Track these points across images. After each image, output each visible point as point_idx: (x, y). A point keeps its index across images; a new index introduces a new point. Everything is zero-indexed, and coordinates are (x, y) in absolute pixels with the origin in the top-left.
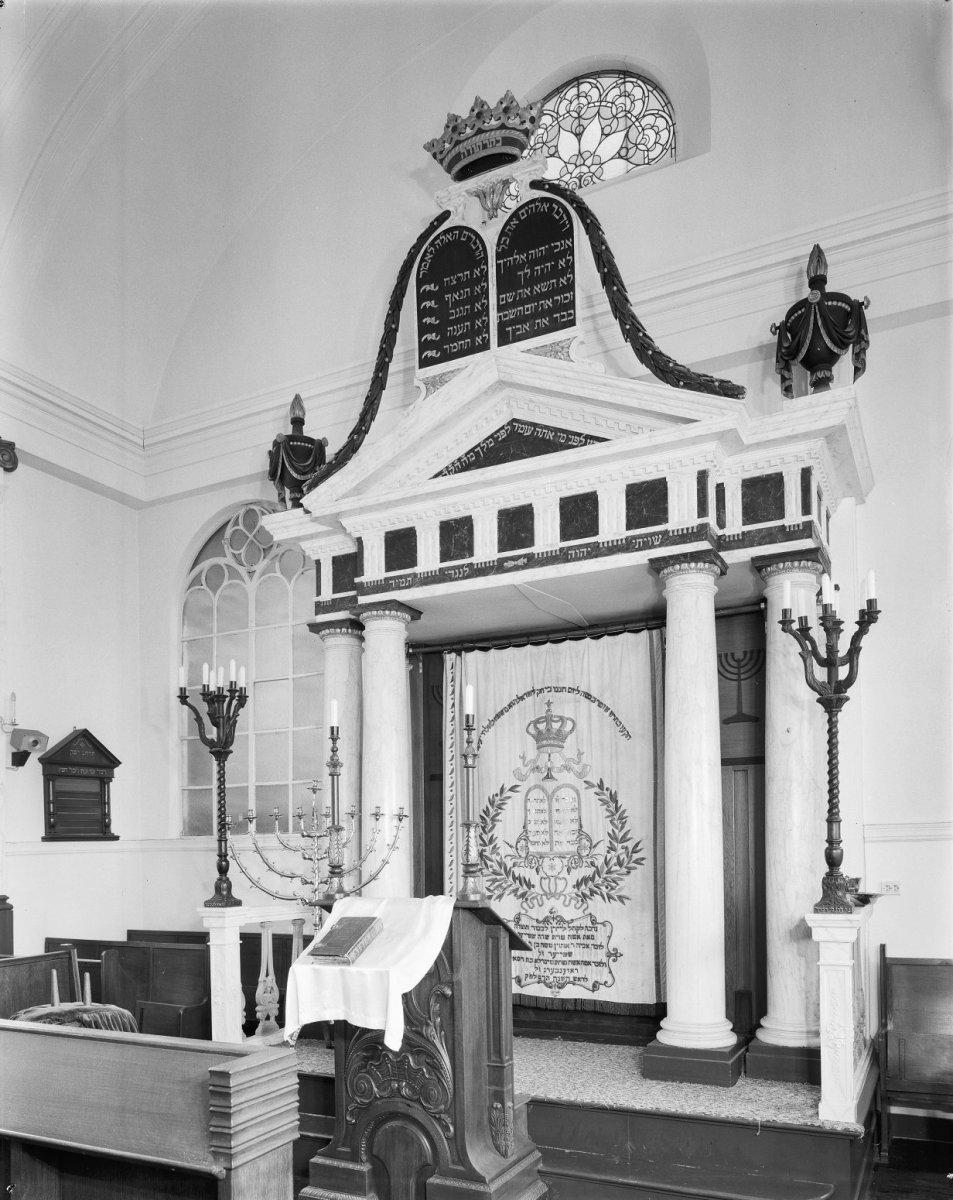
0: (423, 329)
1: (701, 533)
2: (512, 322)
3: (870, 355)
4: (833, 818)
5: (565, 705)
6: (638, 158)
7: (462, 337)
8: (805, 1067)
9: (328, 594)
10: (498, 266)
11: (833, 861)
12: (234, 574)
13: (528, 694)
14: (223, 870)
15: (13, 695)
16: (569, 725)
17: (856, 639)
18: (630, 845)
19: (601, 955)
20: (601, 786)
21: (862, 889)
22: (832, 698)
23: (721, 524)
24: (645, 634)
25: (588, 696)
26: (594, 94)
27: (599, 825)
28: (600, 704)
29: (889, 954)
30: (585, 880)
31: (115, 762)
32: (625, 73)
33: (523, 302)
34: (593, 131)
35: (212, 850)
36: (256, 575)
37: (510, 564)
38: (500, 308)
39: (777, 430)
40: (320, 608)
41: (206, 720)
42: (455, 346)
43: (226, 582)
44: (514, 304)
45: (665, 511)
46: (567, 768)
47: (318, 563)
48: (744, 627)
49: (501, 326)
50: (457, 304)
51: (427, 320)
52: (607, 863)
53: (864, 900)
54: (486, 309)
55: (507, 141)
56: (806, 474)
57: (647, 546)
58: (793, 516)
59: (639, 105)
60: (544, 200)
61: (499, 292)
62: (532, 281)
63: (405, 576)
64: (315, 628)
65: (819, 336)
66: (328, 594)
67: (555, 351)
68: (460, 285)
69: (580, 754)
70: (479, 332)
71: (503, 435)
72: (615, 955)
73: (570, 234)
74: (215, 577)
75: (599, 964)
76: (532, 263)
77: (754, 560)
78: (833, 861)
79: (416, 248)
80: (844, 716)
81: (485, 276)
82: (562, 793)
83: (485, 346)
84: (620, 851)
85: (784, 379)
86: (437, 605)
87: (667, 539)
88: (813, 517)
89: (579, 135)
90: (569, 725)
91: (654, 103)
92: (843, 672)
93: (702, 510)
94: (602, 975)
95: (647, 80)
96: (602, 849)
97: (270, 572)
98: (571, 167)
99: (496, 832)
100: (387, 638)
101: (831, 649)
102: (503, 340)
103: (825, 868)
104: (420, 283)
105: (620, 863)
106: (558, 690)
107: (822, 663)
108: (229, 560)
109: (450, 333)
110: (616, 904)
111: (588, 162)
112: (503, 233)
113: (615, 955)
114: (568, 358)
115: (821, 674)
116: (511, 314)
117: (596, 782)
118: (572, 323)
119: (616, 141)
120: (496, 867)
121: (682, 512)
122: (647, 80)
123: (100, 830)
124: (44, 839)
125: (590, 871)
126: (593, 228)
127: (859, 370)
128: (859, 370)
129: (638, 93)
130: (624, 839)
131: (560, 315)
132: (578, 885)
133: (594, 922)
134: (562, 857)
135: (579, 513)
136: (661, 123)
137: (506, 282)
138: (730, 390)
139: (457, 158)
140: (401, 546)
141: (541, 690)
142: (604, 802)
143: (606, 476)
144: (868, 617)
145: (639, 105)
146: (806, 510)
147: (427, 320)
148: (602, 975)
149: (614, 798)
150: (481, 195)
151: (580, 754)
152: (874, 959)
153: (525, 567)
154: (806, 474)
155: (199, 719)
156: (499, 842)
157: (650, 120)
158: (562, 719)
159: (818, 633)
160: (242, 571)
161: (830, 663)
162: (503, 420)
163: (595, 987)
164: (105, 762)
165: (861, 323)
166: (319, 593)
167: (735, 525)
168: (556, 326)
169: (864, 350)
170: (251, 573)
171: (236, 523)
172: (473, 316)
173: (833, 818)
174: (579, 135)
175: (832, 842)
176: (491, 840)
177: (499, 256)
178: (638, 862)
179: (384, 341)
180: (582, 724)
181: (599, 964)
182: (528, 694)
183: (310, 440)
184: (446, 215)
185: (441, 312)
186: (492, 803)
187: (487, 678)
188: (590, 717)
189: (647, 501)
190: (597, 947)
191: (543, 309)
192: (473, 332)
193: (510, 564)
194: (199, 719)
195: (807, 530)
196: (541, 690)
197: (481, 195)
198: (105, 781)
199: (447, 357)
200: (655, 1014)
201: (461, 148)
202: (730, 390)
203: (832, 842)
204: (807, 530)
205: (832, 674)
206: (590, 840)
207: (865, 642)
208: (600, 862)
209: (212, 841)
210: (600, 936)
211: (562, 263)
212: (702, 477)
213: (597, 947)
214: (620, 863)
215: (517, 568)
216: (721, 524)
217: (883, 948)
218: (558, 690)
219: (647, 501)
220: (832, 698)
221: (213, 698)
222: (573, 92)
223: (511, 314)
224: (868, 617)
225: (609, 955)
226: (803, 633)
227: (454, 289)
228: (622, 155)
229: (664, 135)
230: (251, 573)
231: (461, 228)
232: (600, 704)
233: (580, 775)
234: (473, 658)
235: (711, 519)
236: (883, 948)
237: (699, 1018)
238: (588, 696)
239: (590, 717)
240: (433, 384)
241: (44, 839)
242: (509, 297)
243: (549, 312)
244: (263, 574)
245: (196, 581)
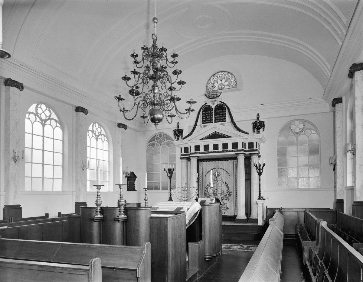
0: (203, 118)
1: (242, 150)
2: (216, 120)
3: (265, 128)
4: (260, 189)
5: (220, 171)
6: (231, 86)
7: (209, 120)
8: (256, 221)
9: (183, 153)
10: (215, 112)
11: (260, 194)
12: (157, 145)
13: (214, 169)
14: (171, 195)
15: (127, 167)
16: (220, 174)
17: (263, 167)
18: (230, 192)
19: (225, 208)
20: (225, 183)
21: (264, 198)
22: (260, 174)
23: (245, 148)
24: (232, 161)
25: (223, 169)
26: (224, 75)
27: (225, 189)
28: (225, 171)
29: (268, 207)
30: (223, 197)
31: (136, 177)
32: (229, 73)
33: (218, 117)
34: (223, 81)
35: (96, 194)
36: (162, 145)
37: (215, 152)
38: (215, 117)
39: (253, 137)
40: (181, 155)
41: (168, 173)
42: (208, 122)
43: (155, 146)
44: (217, 117)
45: (238, 147)
46: (220, 180)
47: (181, 148)
48: (248, 160)
49: (215, 120)
50: (208, 116)
51: (203, 117)
52: (226, 195)
53: (264, 199)
54: (213, 117)
55: (217, 96)
56: (257, 143)
57: (235, 151)
58: (255, 148)
59: (231, 78)
60: (221, 104)
61: (215, 115)
62: (220, 115)
63: (198, 152)
64: (181, 158)
65: (258, 126)
66: (183, 153)
67: (223, 125)
68: (209, 113)
69: (222, 178)
70: (212, 120)
71: (214, 133)
72: (227, 208)
73: (225, 109)
74: (153, 145)
75: (225, 210)
76: (220, 112)
77: (250, 154)
78: (260, 194)
79: (201, 108)
80: (261, 176)
81: (213, 113)
82: (219, 184)
83: (212, 122)
84: (228, 193)
85: (254, 130)
86: (200, 156)
87: (238, 151)
88: (257, 149)
89: (221, 81)
90: (220, 174)
91: (233, 78)
92: (261, 171)
93: (243, 148)
94: (226, 211)
95: (232, 74)
96: (225, 193)
97: (153, 141)
98: (220, 85)
99: (208, 190)
100: (194, 161)
101: (260, 168)
102: (215, 122)
103: (259, 195)
104: (202, 112)
105: (228, 195)
106: (219, 168)
107: (259, 170)
108: (156, 142)
109: (207, 120)
110: (228, 201)
111: (223, 85)
112: (215, 107)
113: (227, 208)
114: (225, 126)
115: (258, 171)
116: (216, 119)
117: (225, 182)
118: (225, 121)
119: (227, 83)
120: (208, 195)
121: (240, 147)
122: (232, 74)
123: (134, 190)
124: (127, 191)
125: (224, 196)
126: (229, 109)
127: (263, 130)
128: (263, 130)
129: (231, 76)
130: (229, 191)
131: (224, 120)
132: (222, 198)
133: (224, 203)
134: (219, 194)
135: (225, 146)
136: (234, 81)
137: (216, 114)
138: (247, 133)
139: (209, 97)
140: (197, 148)
141: (216, 168)
142: (226, 186)
143: (229, 142)
144: (264, 165)
145: (231, 78)
146: (257, 147)
147: (203, 117)
148: (226, 211)
149: (227, 185)
150: (212, 101)
151: (222, 178)
152: (266, 208)
153: (217, 153)
154: (257, 143)
155: (167, 173)
156: (209, 191)
157: (232, 81)
158: (219, 173)
159: (258, 166)
160: (159, 144)
161: (260, 170)
162: (214, 131)
163: (224, 213)
164: (134, 177)
165: (264, 124)
166: (181, 153)
167: (247, 149)
168: (223, 121)
169: (264, 128)
170: (161, 145)
171: (158, 136)
172: (211, 118)
173: (260, 189)
174: (221, 81)
175: (260, 192)
176: (207, 191)
177: (215, 110)
178: (231, 194)
179: (196, 119)
180: (222, 173)
181: (225, 210)
182: (214, 169)
183: (181, 130)
184: (207, 103)
185: (206, 116)
186: (207, 185)
187: (207, 166)
188: (224, 173)
189: (235, 145)
190: (225, 207)
191: (221, 118)
192: (211, 120)
193: (215, 152)
194: (167, 173)
195: (257, 150)
196: (216, 168)
197: (212, 101)
198: (134, 180)
199: (206, 123)
200: (235, 216)
201: (210, 96)
202: (247, 133)
203: (260, 192)
204: (257, 150)
205: (260, 171)
206: (223, 191)
207: (264, 168)
208: (225, 194)
209: (168, 191)
210: (225, 206)
211: (224, 113)
212: (243, 143)
213: (225, 207)
214: (228, 195)
215: (216, 153)
216: (245, 148)
217: (267, 206)
218: (219, 168)
219: (235, 145)
220: (260, 174)
221: (169, 170)
222: (220, 74)
223: (216, 119)
224: (264, 165)
225: (227, 208)
226: (257, 166)
227: (208, 114)
228: (228, 85)
229: (235, 84)
230: (161, 145)
231: (209, 105)
232: (225, 171)
233: (222, 181)
234: (205, 163)
235: (244, 149)
236: (267, 206)
237: (242, 215)
238: (223, 169)
239: (224, 173)
240: (205, 126)
241: (127, 191)
242: (216, 116)
243: (222, 119)
244: (163, 145)
245: (149, 145)
